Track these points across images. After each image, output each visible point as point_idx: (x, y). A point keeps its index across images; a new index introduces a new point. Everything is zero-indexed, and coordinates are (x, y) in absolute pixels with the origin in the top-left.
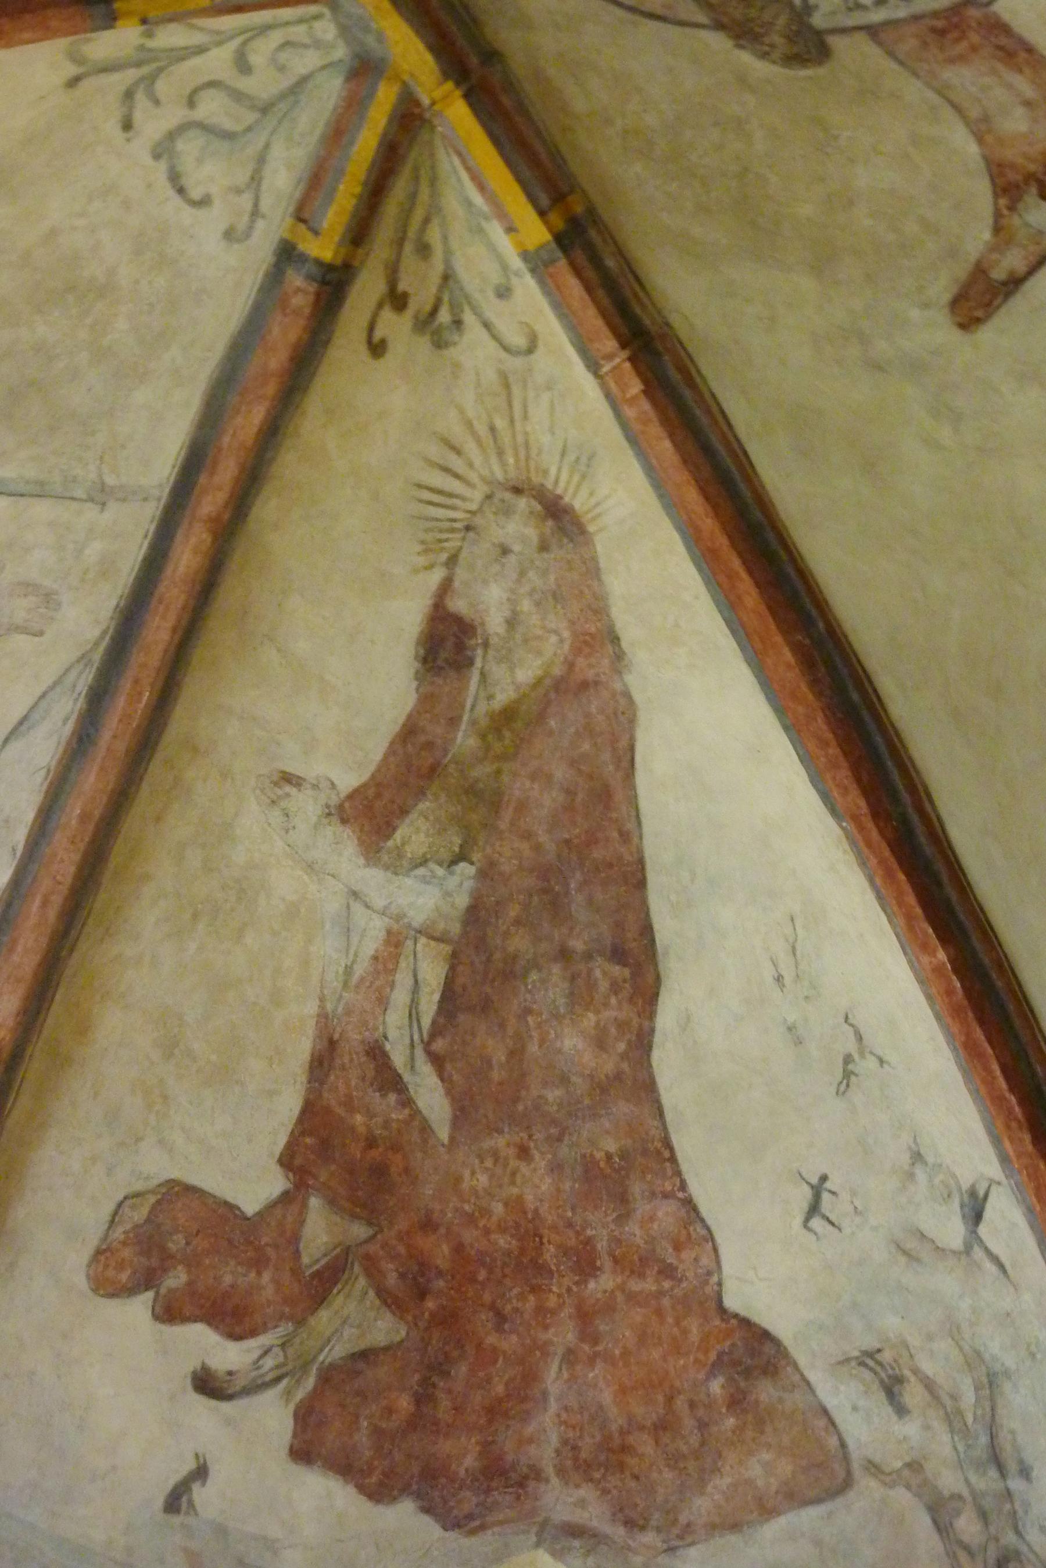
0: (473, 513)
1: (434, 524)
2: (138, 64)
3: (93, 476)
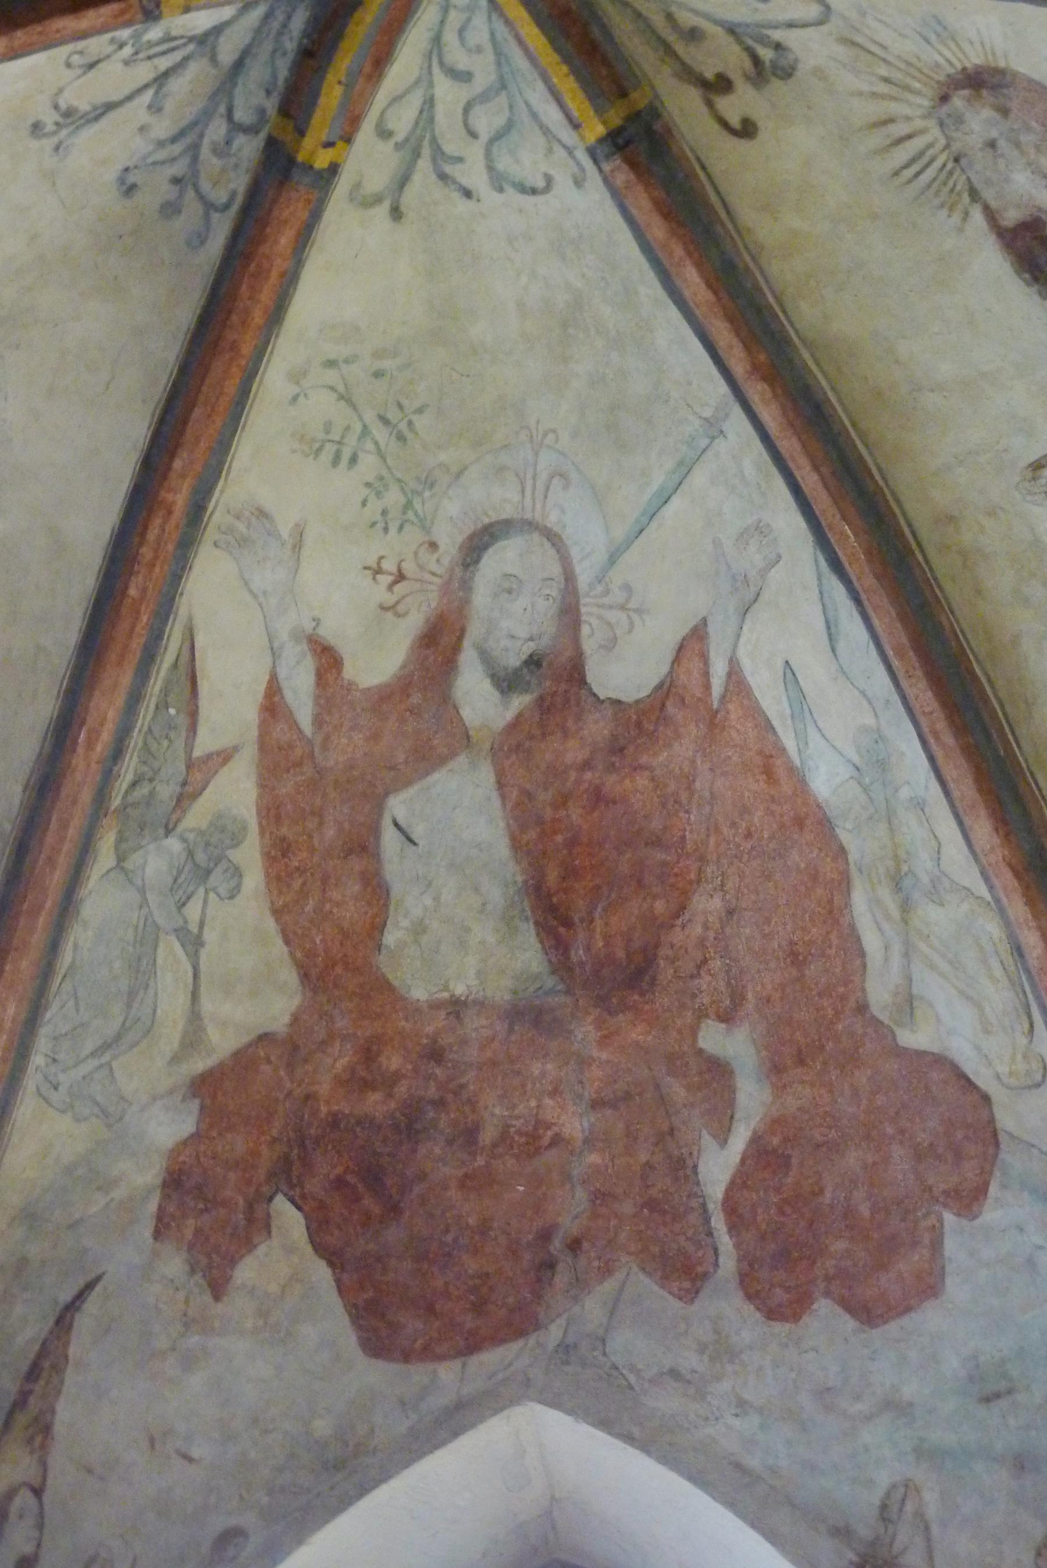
0: (947, 147)
1: (936, 184)
2: (417, 154)
3: (697, 423)
